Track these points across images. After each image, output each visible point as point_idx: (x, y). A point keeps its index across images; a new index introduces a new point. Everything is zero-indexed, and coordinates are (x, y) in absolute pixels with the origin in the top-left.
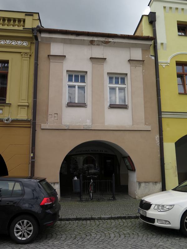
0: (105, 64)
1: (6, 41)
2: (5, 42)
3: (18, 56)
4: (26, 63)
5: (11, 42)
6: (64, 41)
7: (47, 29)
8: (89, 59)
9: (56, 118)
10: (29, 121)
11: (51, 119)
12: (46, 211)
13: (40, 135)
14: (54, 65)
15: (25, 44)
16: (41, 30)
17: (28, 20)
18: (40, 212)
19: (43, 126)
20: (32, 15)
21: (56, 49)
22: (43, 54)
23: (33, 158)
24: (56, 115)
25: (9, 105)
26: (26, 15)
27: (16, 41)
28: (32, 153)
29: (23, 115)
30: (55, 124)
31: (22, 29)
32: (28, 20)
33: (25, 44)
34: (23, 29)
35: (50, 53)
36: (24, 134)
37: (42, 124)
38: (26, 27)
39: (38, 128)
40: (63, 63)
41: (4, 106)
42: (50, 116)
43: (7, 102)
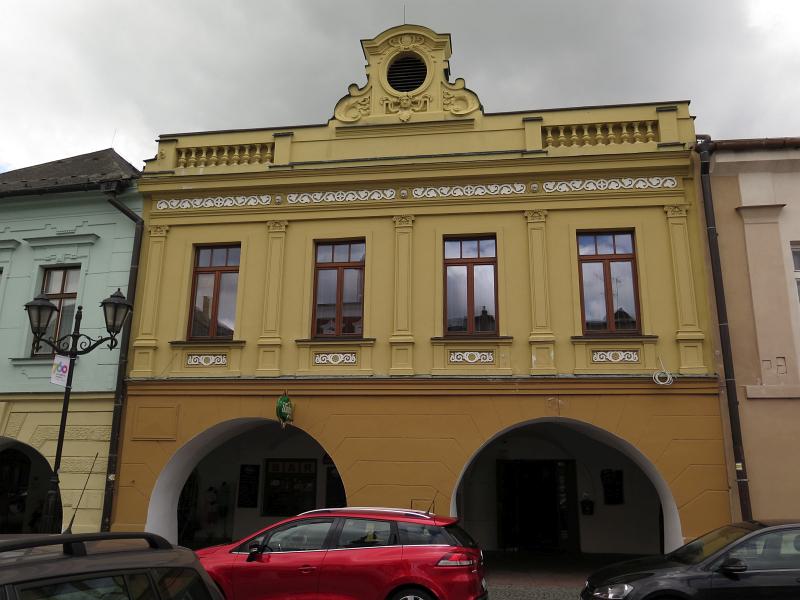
0: (781, 221)
1: (623, 180)
2: (621, 185)
3: (386, 225)
4: (679, 232)
5: (634, 182)
6: (775, 168)
7: (792, 139)
8: (733, 210)
9: (782, 369)
10: (715, 379)
11: (769, 373)
12: (63, 531)
13: (745, 411)
14: (755, 232)
15: (669, 184)
16: (710, 148)
17: (666, 121)
18: (484, 583)
19: (753, 390)
20: (674, 110)
21: (754, 190)
22: (722, 206)
23: (741, 474)
24: (781, 362)
25: (653, 339)
26: (659, 111)
27: (646, 180)
28: (737, 462)
29: (695, 363)
30: (782, 384)
31: (267, 169)
32: (666, 121)
33: (669, 184)
34: (660, 146)
35: (740, 201)
36: (709, 415)
37: (760, 383)
38: (664, 140)
39: (740, 398)
40: (776, 223)
41: (497, 344)
42: (765, 365)
43: (647, 331)
